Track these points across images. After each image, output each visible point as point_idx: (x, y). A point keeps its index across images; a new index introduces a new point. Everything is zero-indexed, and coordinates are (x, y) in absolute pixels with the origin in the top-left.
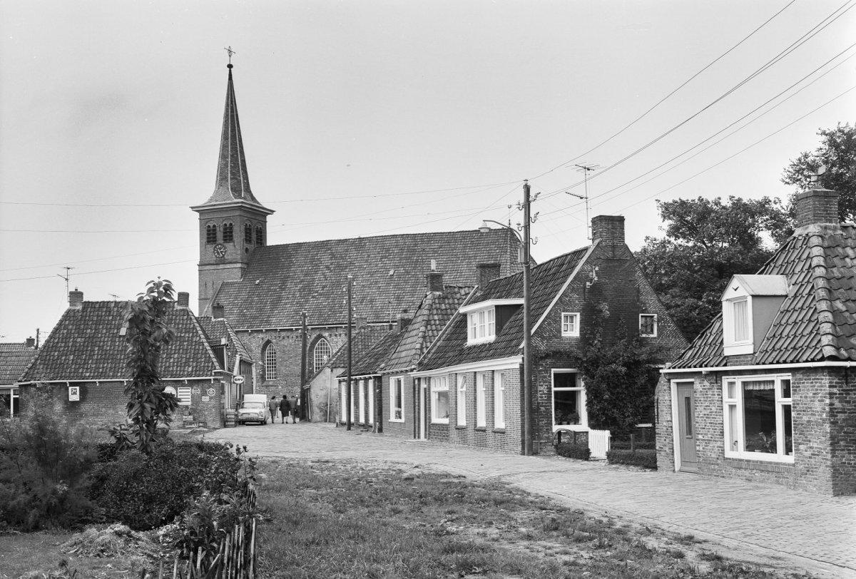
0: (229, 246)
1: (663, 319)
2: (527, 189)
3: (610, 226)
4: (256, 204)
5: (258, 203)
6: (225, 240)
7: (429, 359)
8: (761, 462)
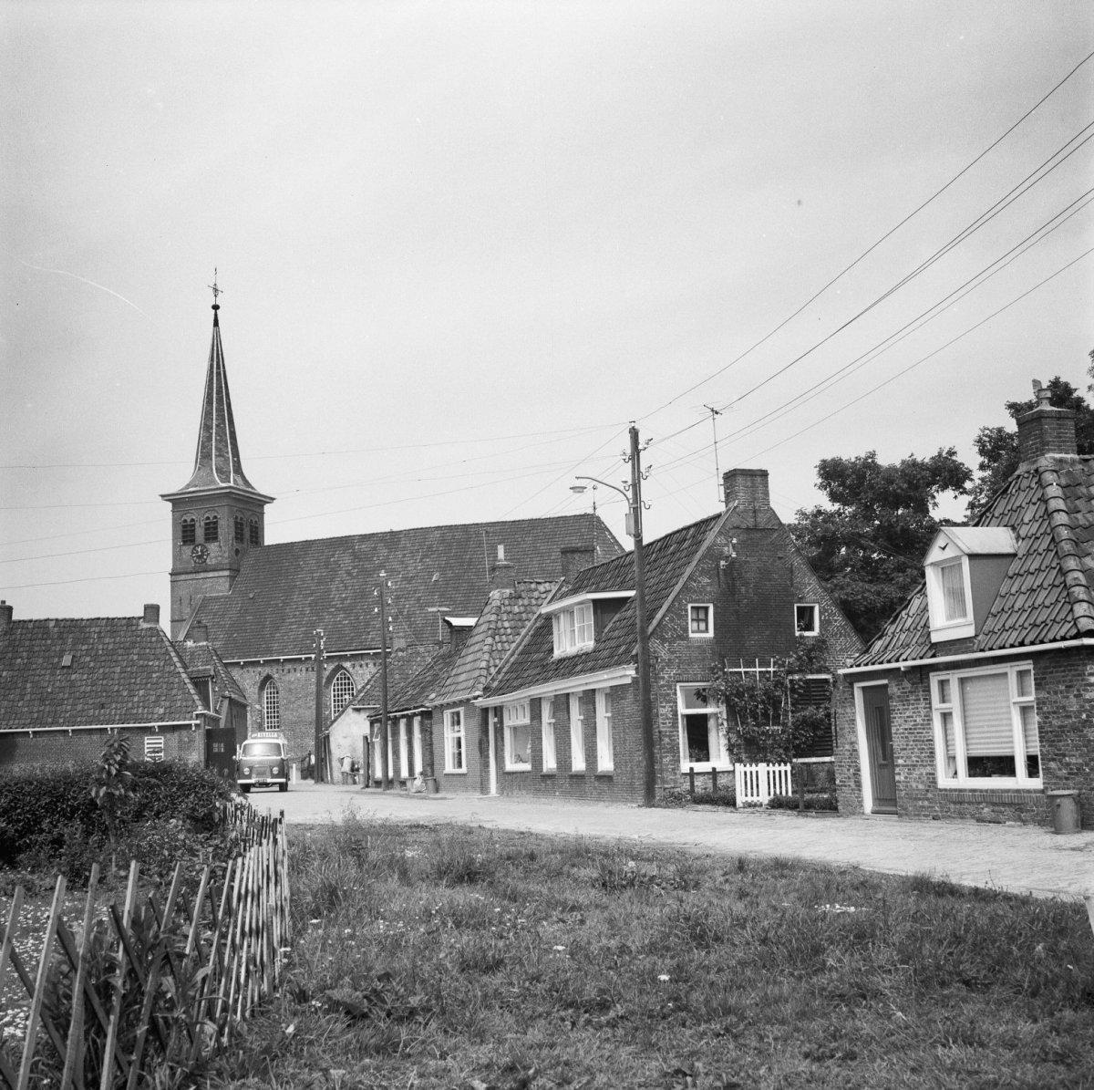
0: (213, 547)
1: (827, 611)
2: (634, 434)
3: (746, 483)
4: (250, 490)
5: (253, 488)
7: (501, 681)
8: (993, 791)
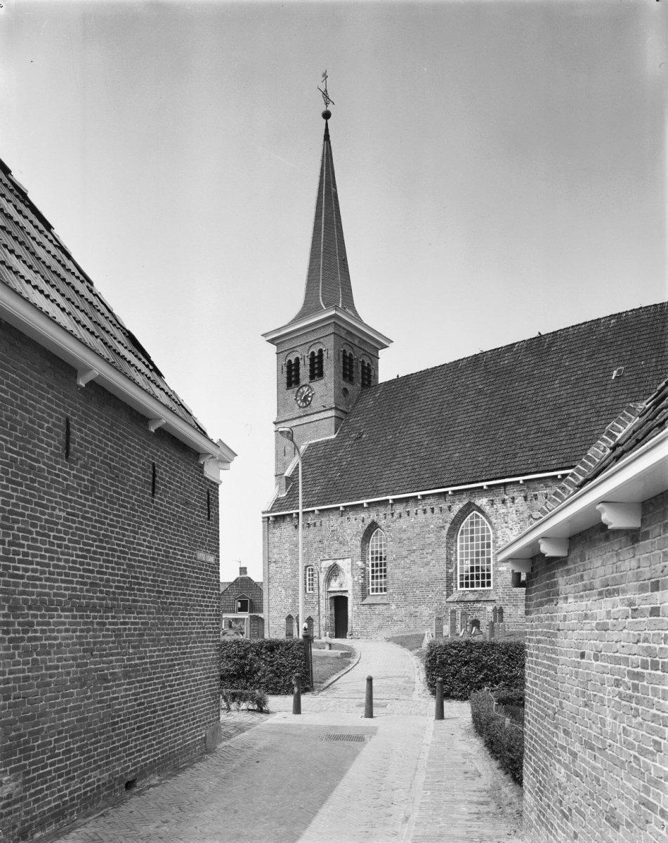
0: (317, 386)
5: (361, 321)
6: (312, 377)
